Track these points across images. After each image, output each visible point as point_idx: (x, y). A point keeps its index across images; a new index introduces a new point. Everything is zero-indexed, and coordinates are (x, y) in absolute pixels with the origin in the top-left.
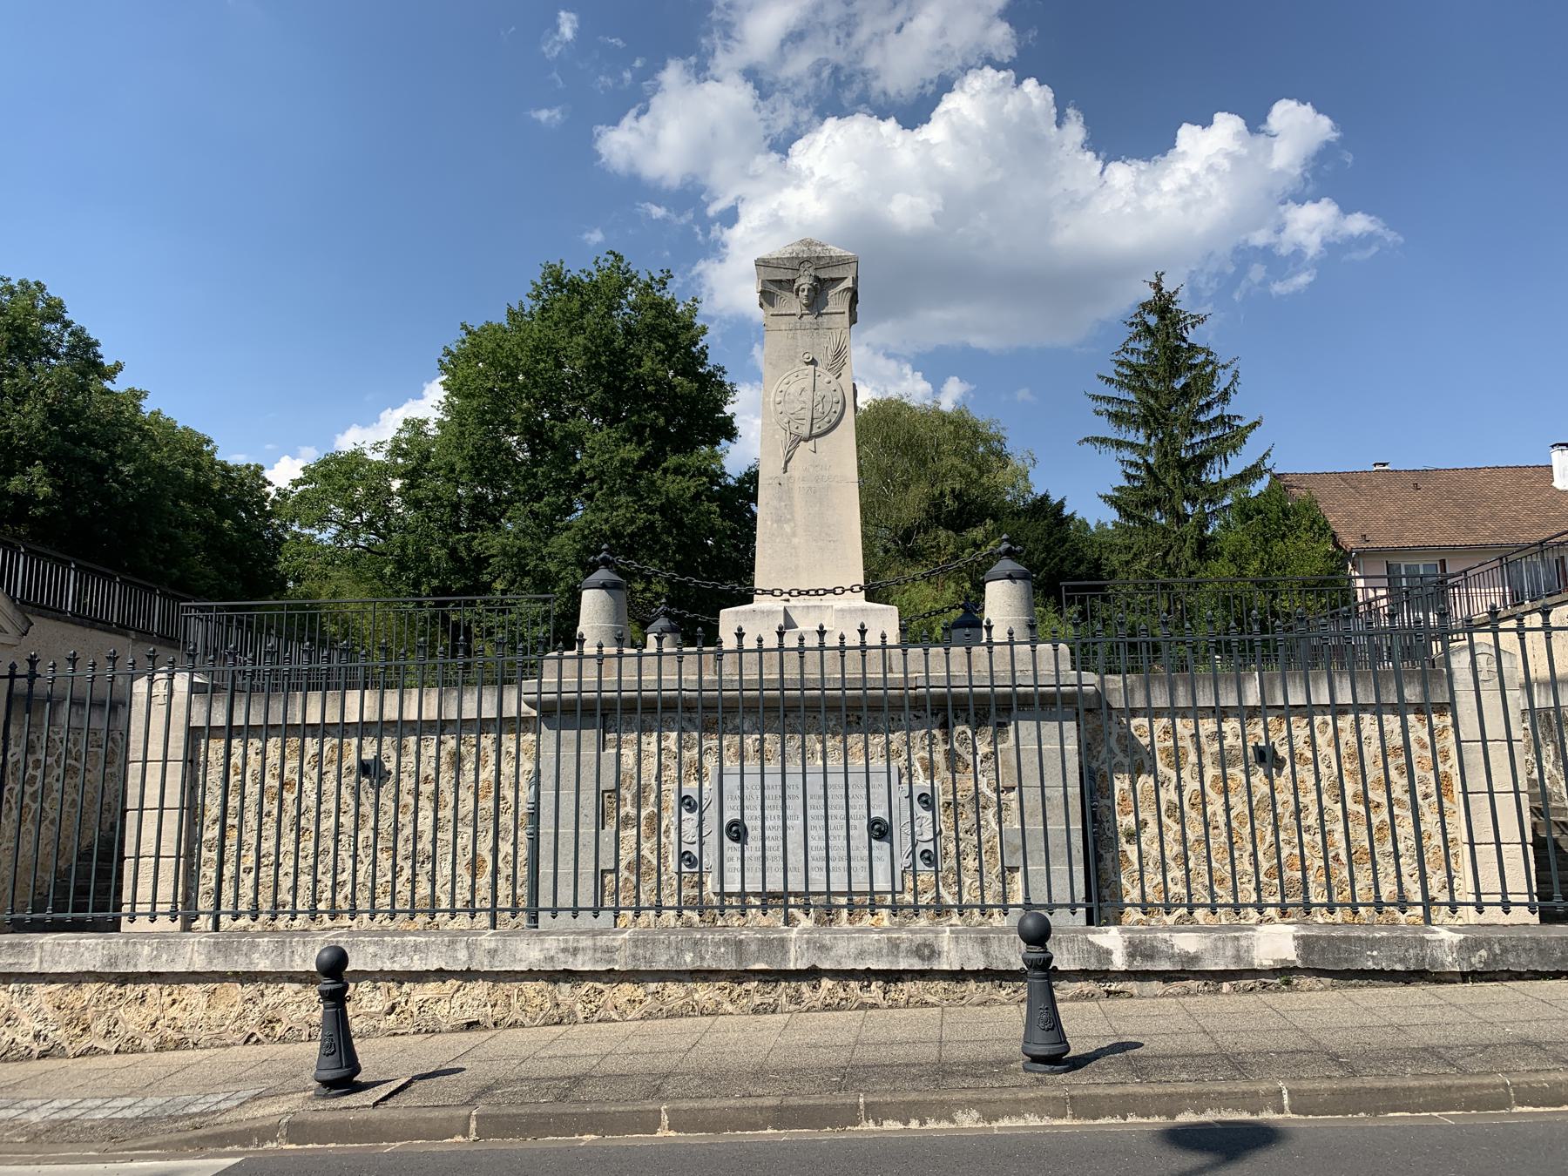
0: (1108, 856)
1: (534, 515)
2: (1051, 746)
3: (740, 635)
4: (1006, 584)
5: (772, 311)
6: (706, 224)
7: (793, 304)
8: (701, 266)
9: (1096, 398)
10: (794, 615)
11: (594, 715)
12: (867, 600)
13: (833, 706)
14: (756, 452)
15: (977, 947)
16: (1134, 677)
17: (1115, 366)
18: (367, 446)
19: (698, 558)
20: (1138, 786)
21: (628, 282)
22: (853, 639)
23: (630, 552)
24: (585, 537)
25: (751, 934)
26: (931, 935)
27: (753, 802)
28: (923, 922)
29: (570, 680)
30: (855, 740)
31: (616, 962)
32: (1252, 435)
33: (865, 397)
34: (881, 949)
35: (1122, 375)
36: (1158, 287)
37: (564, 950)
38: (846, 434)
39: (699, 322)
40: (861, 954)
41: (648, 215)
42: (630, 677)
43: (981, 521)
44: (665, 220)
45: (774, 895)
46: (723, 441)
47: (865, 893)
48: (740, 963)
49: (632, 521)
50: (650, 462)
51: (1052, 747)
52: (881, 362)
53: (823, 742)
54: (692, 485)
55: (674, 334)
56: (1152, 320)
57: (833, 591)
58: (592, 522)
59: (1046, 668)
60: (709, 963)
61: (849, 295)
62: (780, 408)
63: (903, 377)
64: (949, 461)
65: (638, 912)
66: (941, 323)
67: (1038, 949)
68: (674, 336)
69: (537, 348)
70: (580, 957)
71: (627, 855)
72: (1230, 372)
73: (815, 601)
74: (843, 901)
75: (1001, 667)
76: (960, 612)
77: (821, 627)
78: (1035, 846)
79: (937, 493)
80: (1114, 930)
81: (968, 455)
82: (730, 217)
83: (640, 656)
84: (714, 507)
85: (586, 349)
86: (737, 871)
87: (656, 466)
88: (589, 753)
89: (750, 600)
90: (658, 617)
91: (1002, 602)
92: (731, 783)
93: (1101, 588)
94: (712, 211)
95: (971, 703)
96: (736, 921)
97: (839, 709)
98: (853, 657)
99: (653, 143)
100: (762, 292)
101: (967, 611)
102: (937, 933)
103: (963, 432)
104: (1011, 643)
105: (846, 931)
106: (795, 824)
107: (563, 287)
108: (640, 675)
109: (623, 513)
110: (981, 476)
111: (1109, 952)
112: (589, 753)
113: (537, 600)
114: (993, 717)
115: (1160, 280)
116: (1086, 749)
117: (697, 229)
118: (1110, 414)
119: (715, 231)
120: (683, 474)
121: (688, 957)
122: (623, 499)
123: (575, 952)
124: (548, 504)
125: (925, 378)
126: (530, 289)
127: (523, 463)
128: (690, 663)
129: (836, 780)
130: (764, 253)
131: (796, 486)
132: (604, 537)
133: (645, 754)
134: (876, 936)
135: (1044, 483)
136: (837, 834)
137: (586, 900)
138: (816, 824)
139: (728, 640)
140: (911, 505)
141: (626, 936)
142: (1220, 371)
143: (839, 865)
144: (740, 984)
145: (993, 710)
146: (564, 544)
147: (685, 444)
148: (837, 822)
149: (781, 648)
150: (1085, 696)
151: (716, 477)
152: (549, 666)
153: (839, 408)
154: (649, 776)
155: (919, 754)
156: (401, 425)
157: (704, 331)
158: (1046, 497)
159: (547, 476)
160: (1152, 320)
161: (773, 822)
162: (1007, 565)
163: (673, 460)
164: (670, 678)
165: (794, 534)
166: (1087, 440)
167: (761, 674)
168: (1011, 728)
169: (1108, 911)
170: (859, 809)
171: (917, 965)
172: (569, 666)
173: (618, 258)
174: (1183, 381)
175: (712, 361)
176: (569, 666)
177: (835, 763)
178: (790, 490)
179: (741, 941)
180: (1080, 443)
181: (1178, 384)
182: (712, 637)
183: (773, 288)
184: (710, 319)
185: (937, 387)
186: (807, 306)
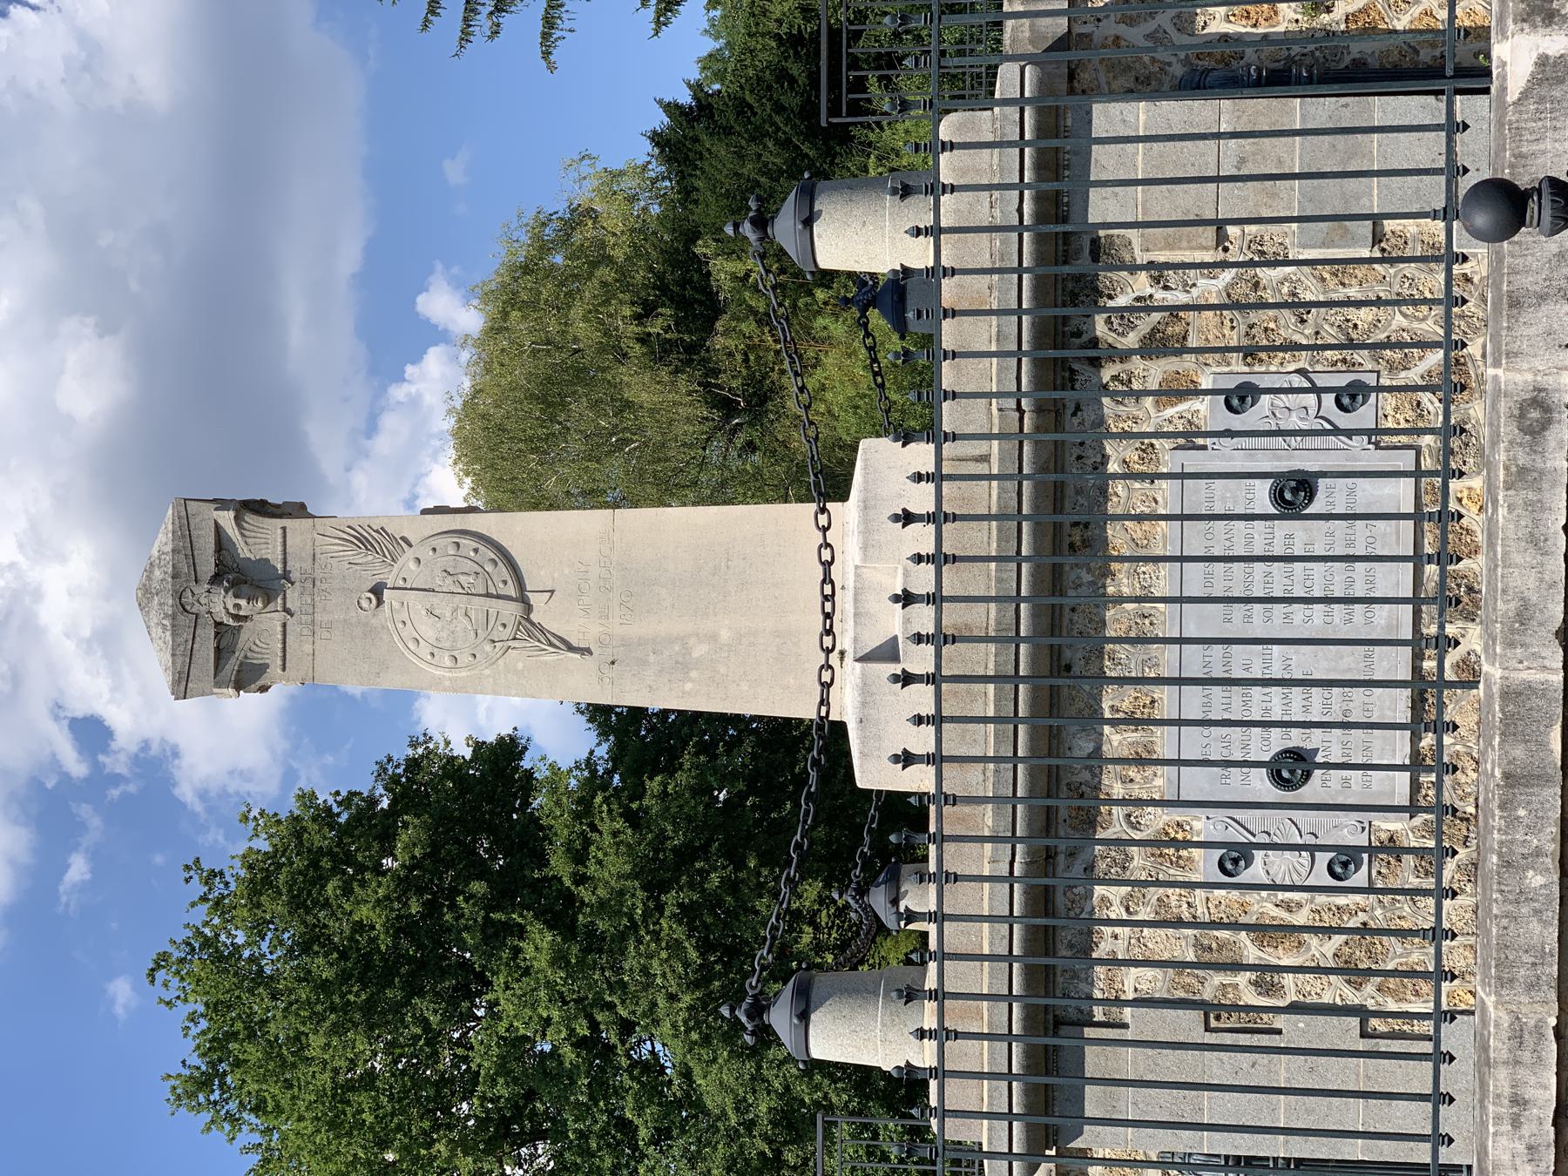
0: (1356, 49)
1: (661, 1136)
2: (1140, 160)
3: (907, 759)
4: (820, 1021)
5: (274, 668)
6: (100, 780)
7: (263, 628)
8: (185, 792)
9: (466, 36)
10: (873, 641)
11: (1056, 1048)
12: (843, 497)
13: (1051, 581)
14: (548, 703)
19: (757, 826)
21: (207, 943)
22: (922, 538)
23: (736, 953)
24: (706, 1040)
25: (1493, 755)
26: (1503, 406)
27: (1235, 744)
28: (1475, 411)
29: (986, 1095)
30: (1119, 537)
33: (448, 483)
34: (1528, 504)
37: (1516, 1123)
38: (524, 531)
39: (290, 806)
41: (82, 888)
42: (983, 978)
43: (699, 263)
44: (95, 856)
45: (1418, 703)
46: (526, 764)
47: (1417, 615)
48: (1547, 780)
49: (675, 947)
50: (560, 912)
52: (382, 444)
53: (1120, 599)
54: (609, 824)
55: (313, 855)
57: (827, 566)
58: (674, 1026)
59: (988, 166)
61: (250, 518)
62: (465, 659)
63: (415, 402)
64: (583, 330)
65: (1443, 974)
66: (311, 329)
67: (1533, 205)
68: (314, 857)
69: (333, 1125)
70: (1529, 1093)
71: (1335, 991)
73: (845, 601)
74: (1431, 570)
75: (982, 250)
76: (874, 315)
77: (896, 599)
78: (1332, 197)
79: (638, 349)
80: (1500, 50)
81: (568, 284)
82: (91, 733)
83: (942, 956)
84: (654, 785)
85: (336, 1030)
86: (1369, 775)
87: (570, 898)
88: (1130, 1063)
89: (840, 729)
90: (868, 909)
91: (857, 237)
92: (1197, 783)
93: (834, 34)
94: (76, 767)
95: (1052, 312)
96: (1468, 777)
97: (1054, 692)
98: (956, 538)
100: (239, 686)
101: (873, 302)
102: (1497, 392)
103: (529, 289)
104: (935, 231)
105: (1492, 570)
106: (1278, 661)
108: (981, 958)
109: (661, 966)
110: (610, 260)
111: (1543, 61)
112: (1130, 1063)
113: (828, 1136)
114: (1082, 265)
116: (1145, 86)
117: (115, 793)
119: (117, 764)
120: (587, 842)
121: (1535, 880)
122: (631, 962)
123: (1518, 1101)
124: (640, 1109)
125: (417, 358)
126: (219, 1136)
127: (557, 1156)
128: (959, 859)
129: (1196, 579)
130: (161, 680)
132: (707, 1004)
133: (1133, 953)
134: (1502, 512)
135: (627, 139)
136: (1301, 579)
137: (1418, 1077)
138: (1274, 621)
139: (919, 780)
140: (661, 397)
141: (1490, 1001)
143: (1359, 579)
145: (1067, 265)
146: (717, 1082)
147: (528, 841)
148: (1278, 579)
149: (933, 679)
150: (1043, 85)
151: (594, 783)
152: (956, 1131)
153: (466, 542)
154: (1181, 946)
155: (1150, 415)
157: (307, 798)
158: (657, 138)
159: (583, 1111)
161: (1275, 703)
162: (785, 228)
163: (559, 865)
164: (987, 899)
165: (713, 637)
166: (546, 55)
167: (985, 720)
169: (1464, 53)
170: (1258, 538)
172: (959, 1095)
173: (162, 961)
175: (365, 783)
176: (959, 1095)
177: (1163, 580)
178: (626, 643)
179: (1507, 776)
180: (552, 67)
182: (905, 812)
183: (231, 666)
184: (289, 775)
185: (435, 335)
186: (268, 600)
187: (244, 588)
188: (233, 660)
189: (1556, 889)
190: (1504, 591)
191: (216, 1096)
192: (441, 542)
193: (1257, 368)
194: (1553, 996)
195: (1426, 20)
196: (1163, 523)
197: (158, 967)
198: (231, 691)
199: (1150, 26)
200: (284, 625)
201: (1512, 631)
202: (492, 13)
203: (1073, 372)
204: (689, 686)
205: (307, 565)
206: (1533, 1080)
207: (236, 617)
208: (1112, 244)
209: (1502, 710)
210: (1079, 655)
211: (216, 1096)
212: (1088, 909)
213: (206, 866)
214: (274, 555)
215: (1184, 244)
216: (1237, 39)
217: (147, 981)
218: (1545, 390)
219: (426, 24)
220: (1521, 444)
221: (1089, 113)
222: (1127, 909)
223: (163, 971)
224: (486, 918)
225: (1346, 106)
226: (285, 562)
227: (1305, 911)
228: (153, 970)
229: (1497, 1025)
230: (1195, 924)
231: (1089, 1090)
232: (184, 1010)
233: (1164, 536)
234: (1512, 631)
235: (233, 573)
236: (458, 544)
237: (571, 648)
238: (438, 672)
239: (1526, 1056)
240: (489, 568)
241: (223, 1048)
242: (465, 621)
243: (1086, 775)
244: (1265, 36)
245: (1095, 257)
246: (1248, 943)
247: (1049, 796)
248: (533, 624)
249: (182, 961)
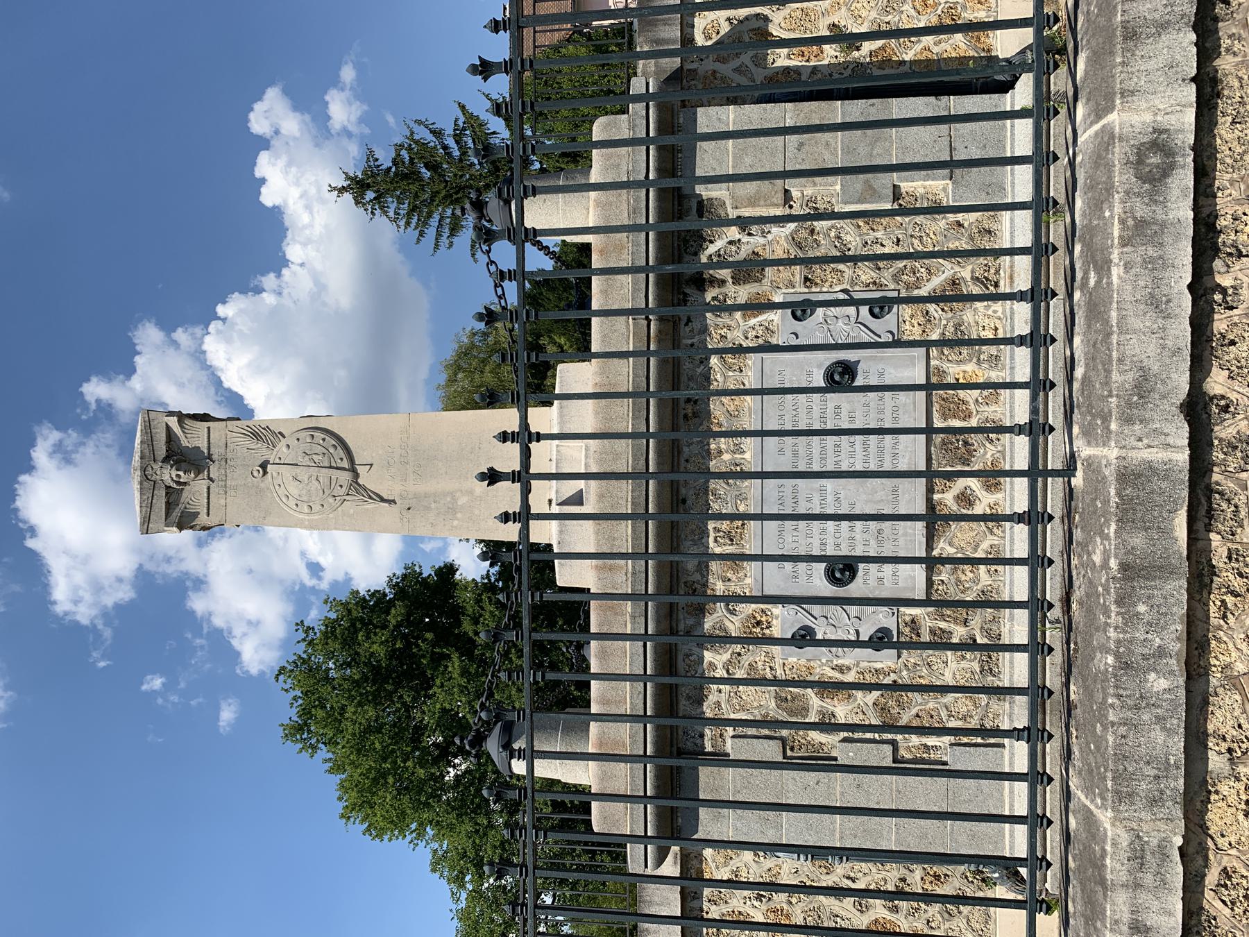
9: (437, 246)
11: (679, 768)
15: (1145, 49)
16: (639, 39)
17: (409, 229)
18: (454, 907)
20: (786, 35)
21: (304, 662)
30: (719, 409)
31: (1162, 847)
32: (471, 108)
34: (1147, 262)
35: (417, 224)
36: (342, 190)
40: (1157, 304)
50: (466, 646)
51: (733, 145)
55: (357, 617)
56: (370, 195)
60: (1172, 637)
62: (316, 508)
70: (1151, 920)
72: (416, 128)
95: (669, 268)
99: (254, 624)
100: (181, 528)
107: (306, 724)
115: (335, 189)
121: (1158, 683)
126: (306, 755)
134: (1116, 272)
142: (416, 137)
144: (1213, 571)
145: (680, 217)
147: (457, 612)
153: (318, 435)
156: (437, 875)
160: (370, 195)
163: (467, 626)
168: (706, 192)
171: (1184, 178)
174: (423, 170)
178: (417, 497)
179: (1124, 567)
181: (426, 174)
183: (176, 513)
186: (199, 472)
187: (183, 465)
189: (1182, 693)
190: (1120, 361)
191: (305, 736)
192: (302, 435)
193: (814, 290)
194: (1178, 812)
195: (925, 53)
196: (748, 398)
197: (280, 673)
198: (175, 529)
199: (736, 63)
200: (209, 488)
201: (1130, 405)
203: (685, 295)
204: (456, 523)
205: (222, 451)
206: (1155, 905)
207: (178, 483)
208: (712, 204)
209: (1119, 494)
210: (691, 492)
211: (305, 736)
212: (700, 671)
213: (306, 624)
215: (762, 203)
216: (797, 70)
218: (1167, 130)
219: (418, 241)
220: (1139, 194)
221: (695, 114)
222: (728, 671)
225: (873, 105)
227: (853, 672)
229: (1114, 845)
230: (775, 682)
231: (703, 813)
232: (292, 693)
233: (750, 408)
234: (1130, 405)
235: (179, 456)
237: (383, 500)
238: (301, 516)
239: (1148, 879)
240: (332, 450)
241: (310, 713)
242: (316, 483)
243: (697, 577)
244: (815, 67)
245: (701, 215)
246: (813, 695)
247: (671, 593)
249: (292, 671)
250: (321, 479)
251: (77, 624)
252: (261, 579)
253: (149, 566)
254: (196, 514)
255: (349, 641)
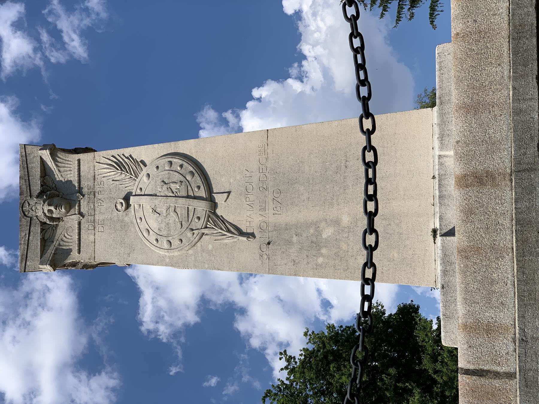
9: (399, 19)
62: (176, 243)
118: (412, 6)
131: (272, 219)
153: (177, 161)
165: (337, 222)
166: (432, 22)
178: (277, 229)
180: (434, 27)
183: (51, 251)
186: (70, 206)
187: (56, 200)
188: (52, 247)
200: (79, 224)
202: (409, 9)
204: (320, 260)
205: (91, 183)
207: (52, 219)
213: (289, 353)
214: (73, 177)
217: (262, 402)
223: (268, 398)
224: (395, 385)
226: (79, 182)
228: (264, 397)
236: (171, 163)
237: (241, 233)
240: (189, 177)
248: (217, 216)
249: (276, 394)
250: (178, 210)
251: (157, 341)
252: (290, 308)
253: (209, 296)
254: (68, 252)
255: (322, 373)
